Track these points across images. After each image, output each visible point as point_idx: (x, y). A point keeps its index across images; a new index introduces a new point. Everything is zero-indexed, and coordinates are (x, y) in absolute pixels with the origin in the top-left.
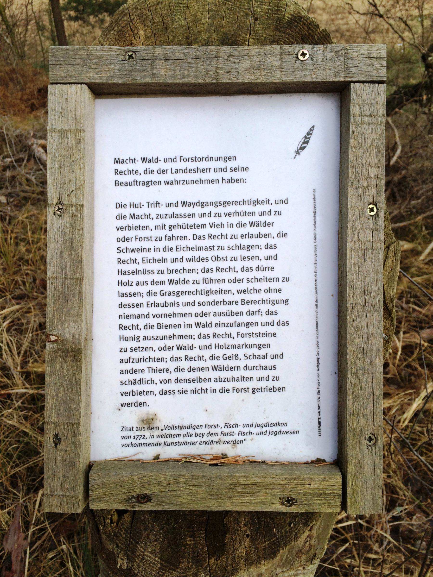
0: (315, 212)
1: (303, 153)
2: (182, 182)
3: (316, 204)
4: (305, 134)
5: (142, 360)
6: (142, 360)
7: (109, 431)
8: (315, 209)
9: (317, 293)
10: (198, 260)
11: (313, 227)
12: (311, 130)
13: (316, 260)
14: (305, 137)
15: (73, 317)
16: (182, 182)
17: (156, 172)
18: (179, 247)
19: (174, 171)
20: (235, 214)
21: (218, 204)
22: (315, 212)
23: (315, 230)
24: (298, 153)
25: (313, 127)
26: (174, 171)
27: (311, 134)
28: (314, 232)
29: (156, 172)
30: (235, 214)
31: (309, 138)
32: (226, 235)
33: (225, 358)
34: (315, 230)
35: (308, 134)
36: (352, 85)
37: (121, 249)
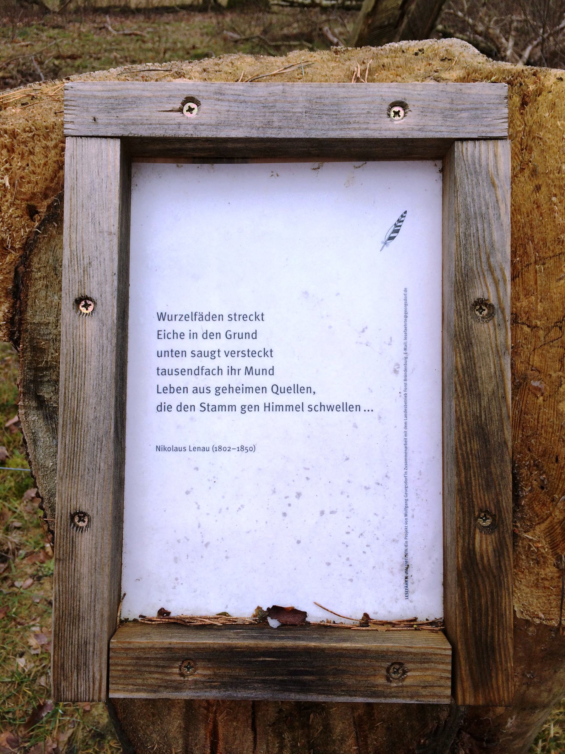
0: (406, 317)
1: (392, 243)
2: (178, 318)
3: (408, 307)
4: (395, 221)
7: (140, 603)
8: (406, 313)
9: (406, 417)
10: (207, 318)
12: (402, 216)
15: (52, 574)
16: (178, 318)
17: (174, 408)
18: (162, 333)
19: (192, 449)
22: (406, 317)
23: (406, 338)
24: (385, 243)
25: (405, 212)
26: (192, 449)
28: (404, 341)
29: (174, 408)
31: (400, 226)
33: (229, 337)
34: (406, 338)
35: (399, 221)
36: (458, 144)
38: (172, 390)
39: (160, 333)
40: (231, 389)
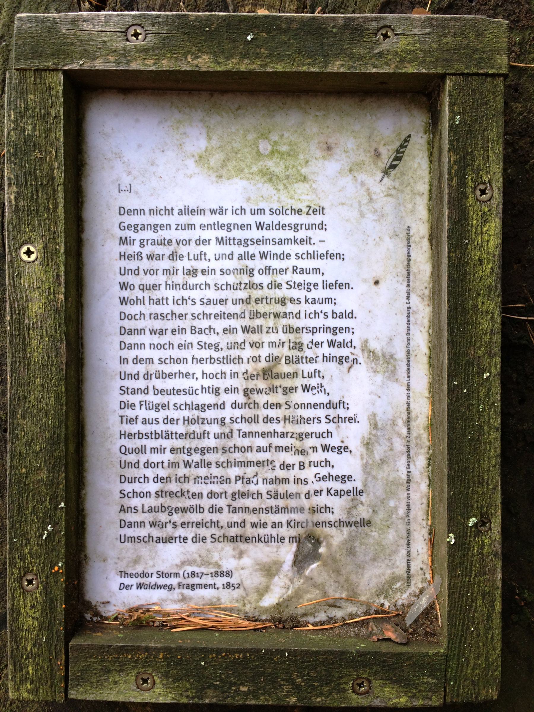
1: (393, 172)
5: (322, 330)
6: (322, 330)
11: (407, 325)
13: (409, 329)
14: (398, 151)
20: (177, 375)
21: (180, 227)
25: (409, 136)
27: (406, 147)
30: (177, 375)
31: (403, 152)
32: (172, 209)
33: (123, 228)
35: (402, 146)
37: (331, 418)
38: (164, 375)
39: (142, 403)
40: (331, 478)
